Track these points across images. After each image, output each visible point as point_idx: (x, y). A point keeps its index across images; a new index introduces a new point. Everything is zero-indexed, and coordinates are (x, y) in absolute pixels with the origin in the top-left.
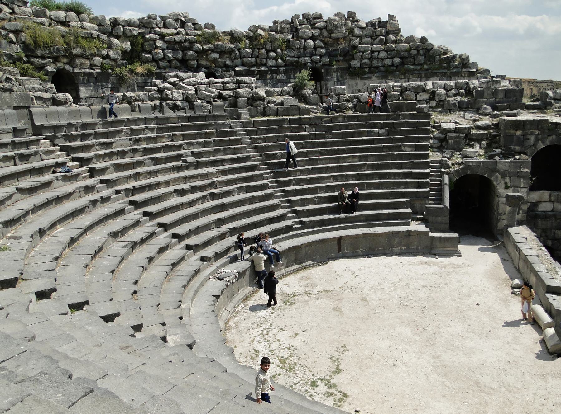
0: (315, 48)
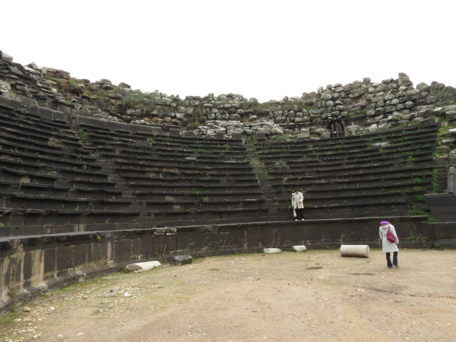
0: (335, 105)
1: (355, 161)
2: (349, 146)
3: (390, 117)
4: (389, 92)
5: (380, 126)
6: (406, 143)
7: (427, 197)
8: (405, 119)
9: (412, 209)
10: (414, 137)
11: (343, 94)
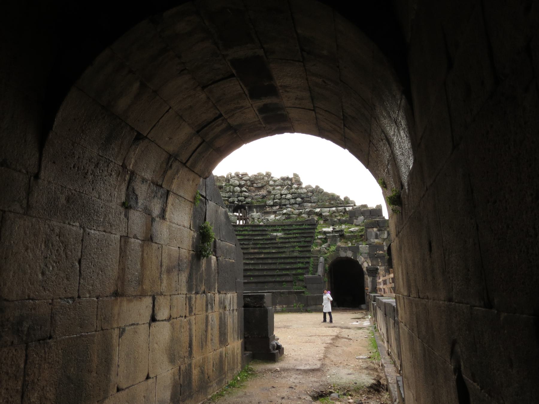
0: (241, 192)
1: (258, 246)
2: (254, 233)
3: (285, 211)
4: (285, 188)
5: (277, 218)
6: (294, 236)
7: (305, 278)
8: (295, 215)
9: (296, 285)
10: (300, 231)
11: (249, 183)
